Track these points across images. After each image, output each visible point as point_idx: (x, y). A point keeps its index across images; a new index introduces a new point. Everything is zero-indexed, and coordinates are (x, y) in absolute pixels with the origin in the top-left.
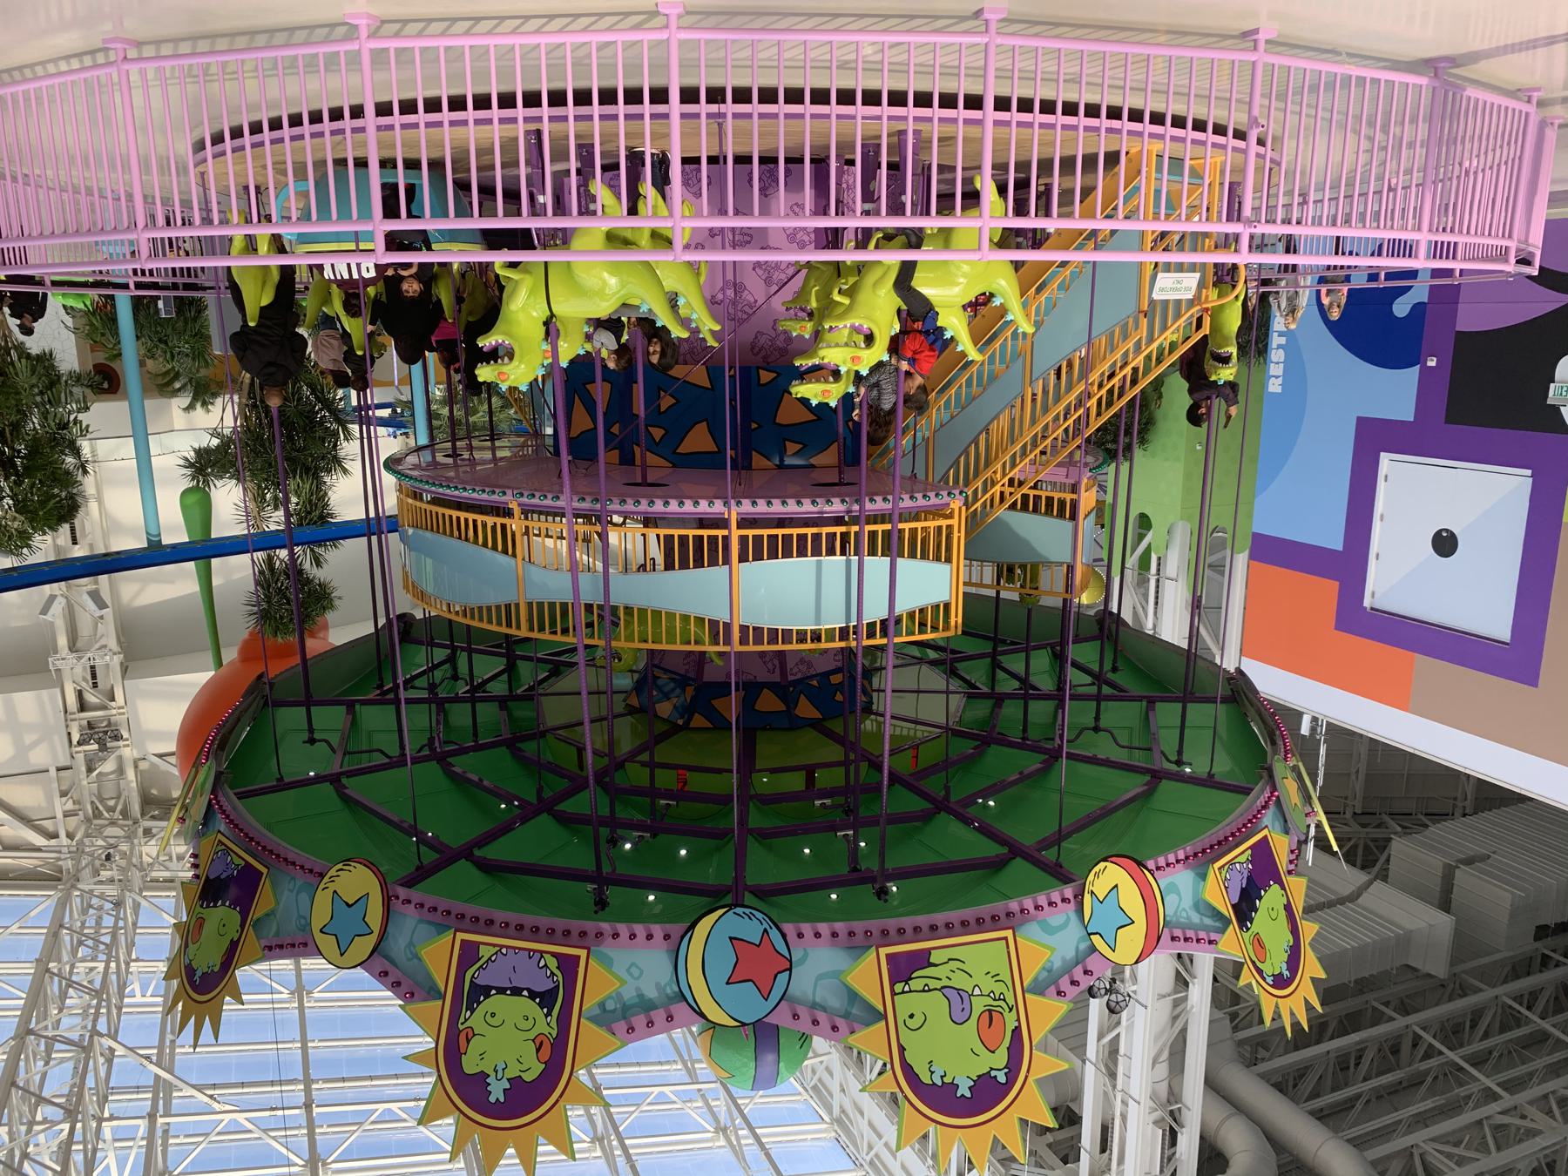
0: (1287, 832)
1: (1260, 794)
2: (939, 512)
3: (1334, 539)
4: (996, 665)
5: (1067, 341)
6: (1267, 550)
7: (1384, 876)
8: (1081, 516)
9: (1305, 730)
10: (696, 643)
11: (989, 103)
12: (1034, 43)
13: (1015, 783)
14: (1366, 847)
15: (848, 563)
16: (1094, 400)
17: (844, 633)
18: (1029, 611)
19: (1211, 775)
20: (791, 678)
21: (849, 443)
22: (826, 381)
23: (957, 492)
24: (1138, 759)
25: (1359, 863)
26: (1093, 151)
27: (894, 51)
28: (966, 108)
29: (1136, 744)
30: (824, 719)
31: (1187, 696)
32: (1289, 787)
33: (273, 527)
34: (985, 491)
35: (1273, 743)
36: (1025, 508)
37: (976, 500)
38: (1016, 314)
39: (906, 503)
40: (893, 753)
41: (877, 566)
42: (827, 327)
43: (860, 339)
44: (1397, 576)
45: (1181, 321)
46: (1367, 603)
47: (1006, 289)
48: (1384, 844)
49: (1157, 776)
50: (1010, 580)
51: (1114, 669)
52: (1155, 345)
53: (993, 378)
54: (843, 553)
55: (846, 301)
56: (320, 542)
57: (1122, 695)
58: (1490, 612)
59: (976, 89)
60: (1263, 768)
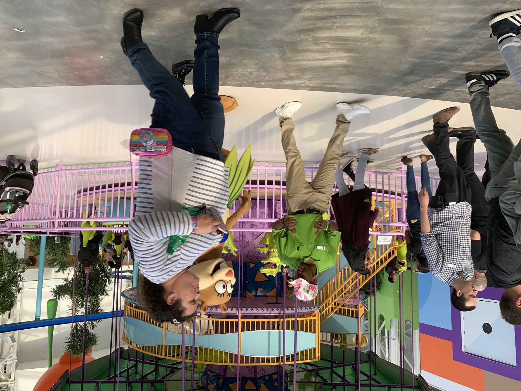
2: (310, 314)
4: (333, 372)
6: (425, 329)
10: (225, 362)
15: (280, 332)
17: (278, 358)
18: (344, 351)
20: (258, 376)
22: (272, 268)
23: (317, 307)
28: (268, 184)
33: (80, 314)
34: (326, 307)
36: (340, 313)
37: (323, 310)
39: (299, 311)
41: (290, 334)
46: (463, 350)
50: (336, 339)
51: (375, 374)
56: (95, 320)
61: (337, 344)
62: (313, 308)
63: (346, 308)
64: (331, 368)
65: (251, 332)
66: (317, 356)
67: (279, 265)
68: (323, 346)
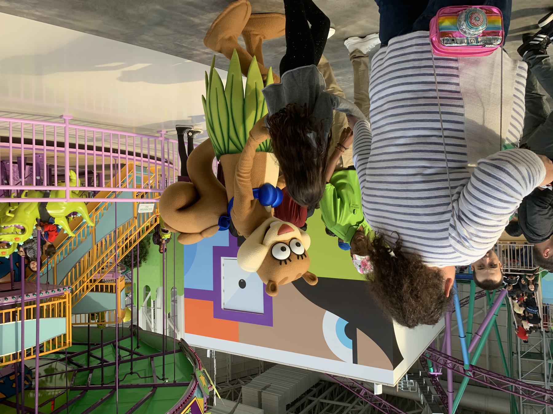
0: (203, 397)
1: (192, 385)
2: (59, 297)
3: (210, 287)
4: (90, 355)
5: (105, 229)
6: (190, 293)
7: (241, 402)
8: (119, 290)
9: (208, 356)
11: (67, 145)
12: (84, 128)
13: (100, 403)
14: (234, 392)
15: (17, 325)
16: (121, 248)
17: (15, 356)
18: (102, 331)
19: (175, 382)
21: (17, 272)
22: (4, 248)
23: (67, 288)
24: (149, 381)
25: (233, 399)
26: (108, 163)
27: (47, 128)
28: (13, 142)
29: (147, 376)
30: (7, 398)
31: (165, 352)
32: (202, 380)
34: (80, 286)
35: (195, 364)
36: (97, 290)
37: (76, 289)
38: (86, 219)
39: (44, 295)
40: (40, 406)
41: (30, 324)
42: (3, 226)
43: (19, 231)
44: (231, 297)
45: (150, 220)
46: (222, 307)
47: (82, 211)
48: (239, 390)
49: (155, 387)
50: (93, 319)
51: (138, 347)
52: (141, 228)
53: (81, 242)
54: (14, 319)
55: (12, 216)
57: (141, 357)
58: (258, 307)
59: (61, 140)
60: (192, 374)
61: (94, 324)
62: (61, 289)
63: (104, 284)
64: (88, 351)
65: (51, 320)
66: (68, 342)
67: (14, 244)
68: (75, 330)
